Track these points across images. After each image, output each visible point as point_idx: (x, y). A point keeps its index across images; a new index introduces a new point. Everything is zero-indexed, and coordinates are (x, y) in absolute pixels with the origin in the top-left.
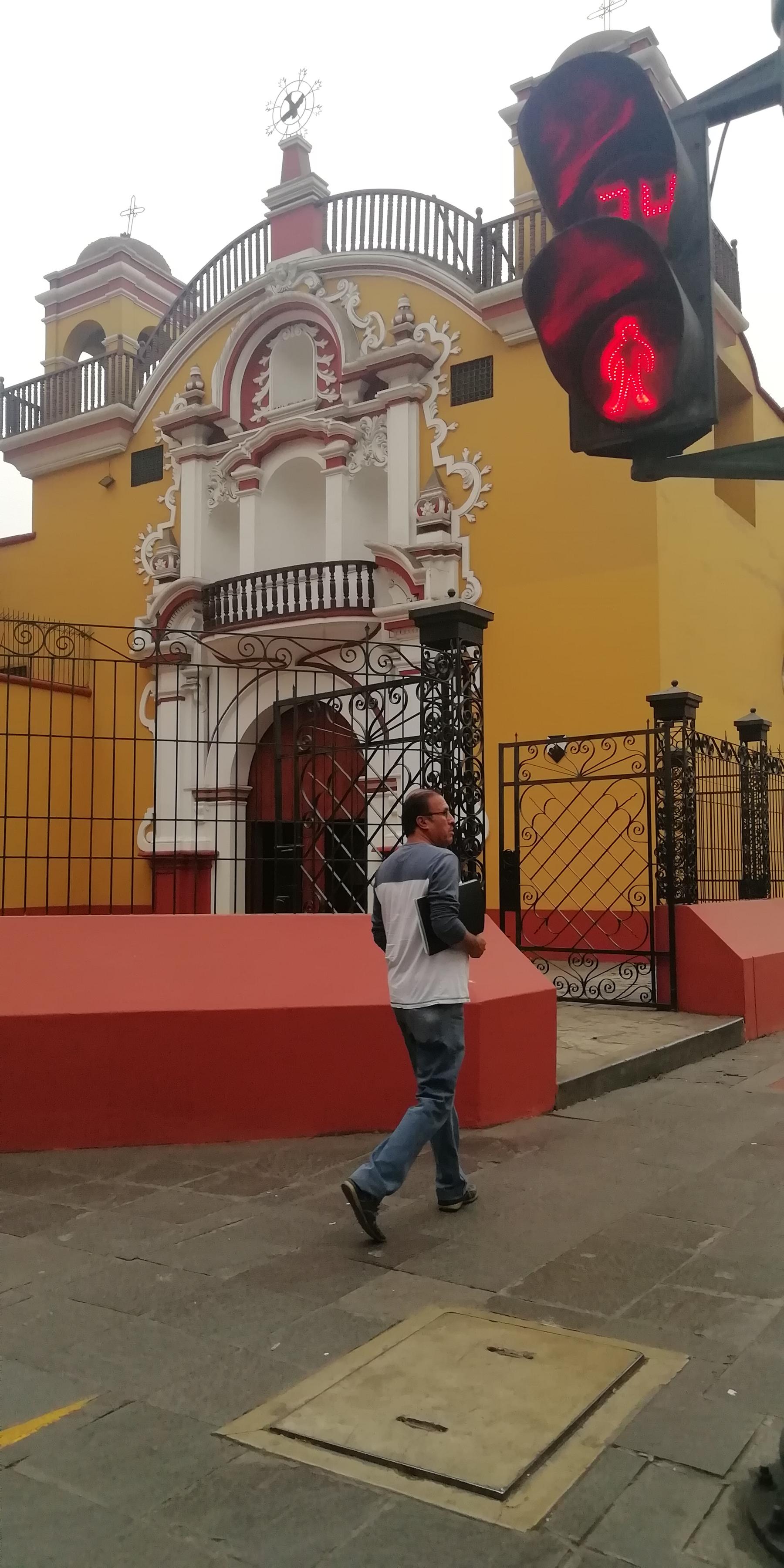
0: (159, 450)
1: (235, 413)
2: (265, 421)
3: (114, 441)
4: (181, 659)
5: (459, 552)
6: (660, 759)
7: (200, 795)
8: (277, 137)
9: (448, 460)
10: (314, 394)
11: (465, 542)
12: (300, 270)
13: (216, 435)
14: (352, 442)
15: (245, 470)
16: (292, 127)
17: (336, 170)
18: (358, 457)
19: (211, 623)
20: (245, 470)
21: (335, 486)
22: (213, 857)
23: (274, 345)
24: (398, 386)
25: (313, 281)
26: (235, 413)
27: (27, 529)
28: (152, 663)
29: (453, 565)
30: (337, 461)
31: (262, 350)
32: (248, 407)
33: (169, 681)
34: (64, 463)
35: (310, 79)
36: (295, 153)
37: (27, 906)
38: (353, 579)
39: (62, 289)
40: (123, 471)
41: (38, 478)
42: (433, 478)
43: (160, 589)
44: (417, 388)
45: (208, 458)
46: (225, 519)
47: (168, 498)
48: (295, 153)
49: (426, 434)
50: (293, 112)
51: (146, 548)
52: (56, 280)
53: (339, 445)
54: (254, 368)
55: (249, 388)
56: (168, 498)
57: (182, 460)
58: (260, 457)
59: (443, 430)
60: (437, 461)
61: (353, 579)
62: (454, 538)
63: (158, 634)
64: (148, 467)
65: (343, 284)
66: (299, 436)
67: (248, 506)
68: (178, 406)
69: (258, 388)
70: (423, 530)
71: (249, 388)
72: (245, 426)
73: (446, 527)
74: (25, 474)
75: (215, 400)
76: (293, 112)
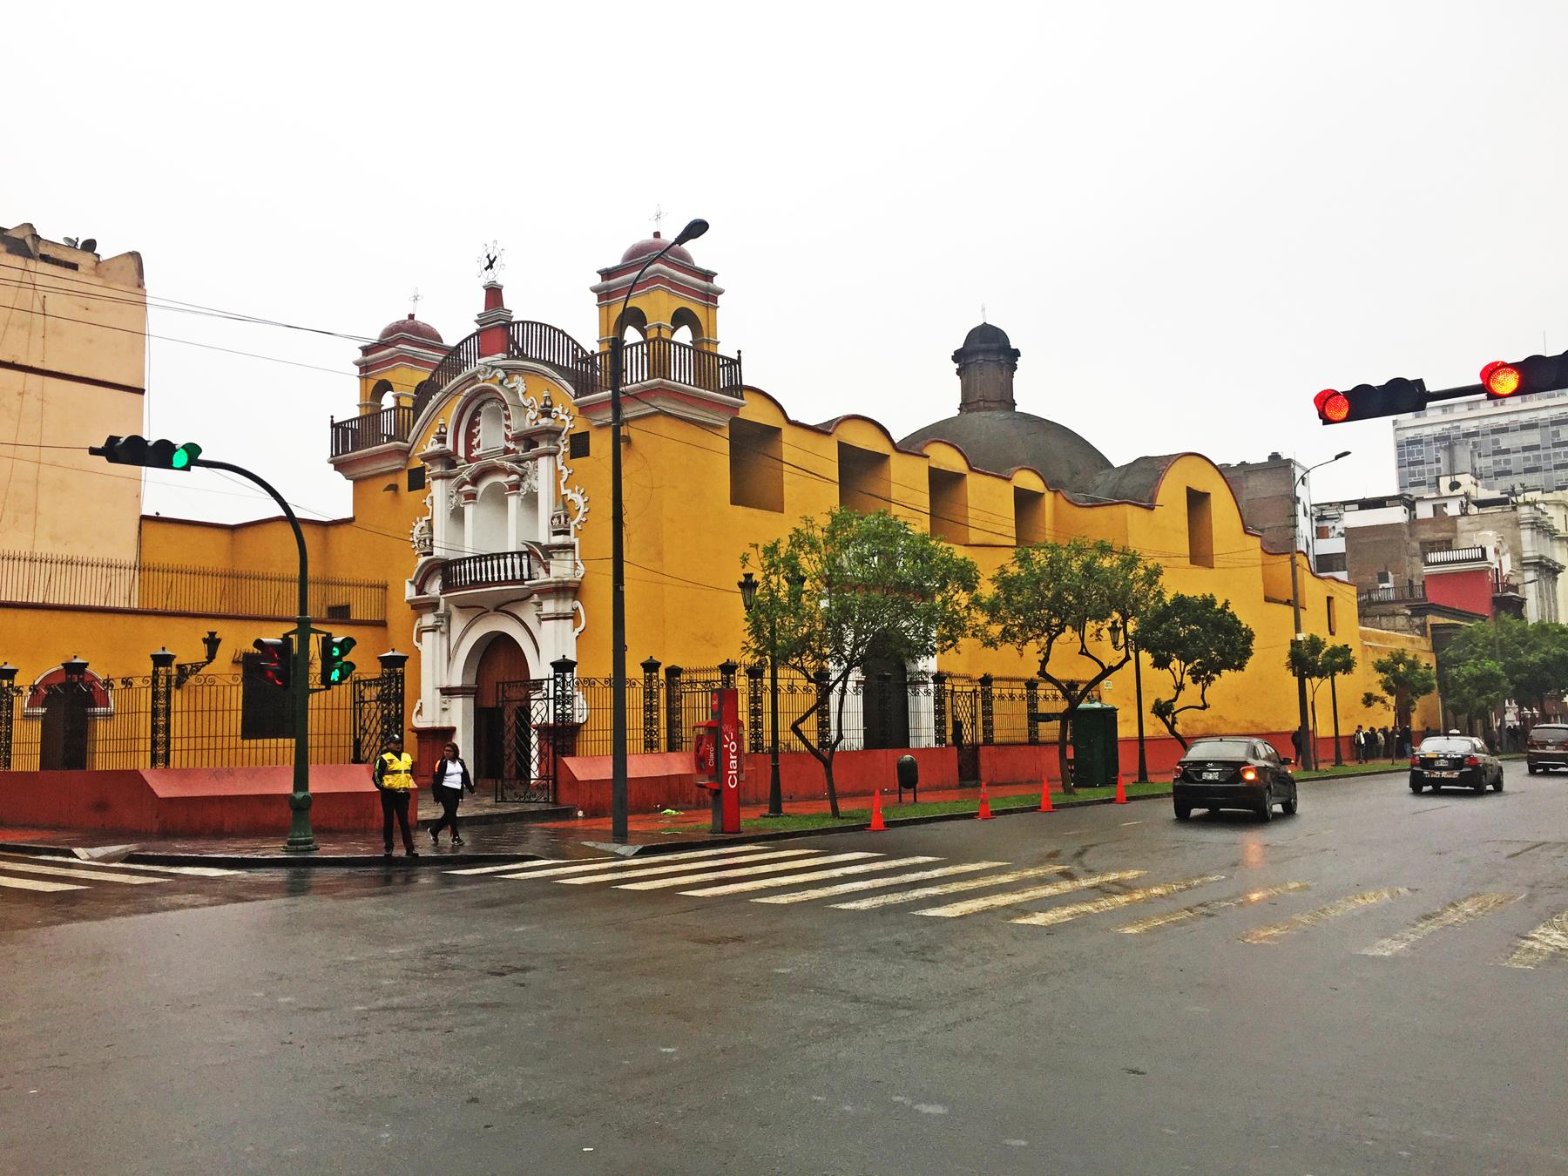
0: (423, 469)
1: (462, 453)
2: (478, 458)
3: (397, 463)
4: (433, 606)
5: (573, 547)
6: (863, 643)
7: (448, 692)
8: (484, 281)
9: (568, 491)
10: (503, 444)
11: (576, 541)
12: (494, 368)
13: (453, 465)
14: (522, 476)
15: (467, 488)
16: (490, 276)
17: (519, 306)
18: (525, 485)
19: (447, 587)
20: (467, 488)
21: (513, 501)
22: (453, 730)
23: (483, 409)
24: (543, 446)
25: (501, 374)
26: (462, 453)
27: (350, 515)
28: (420, 607)
29: (570, 556)
30: (516, 486)
31: (476, 413)
32: (469, 448)
33: (428, 620)
34: (690, 405)
35: (499, 247)
36: (494, 294)
37: (1146, 734)
38: (517, 561)
39: (612, 282)
40: (403, 481)
41: (356, 481)
42: (564, 503)
43: (422, 560)
44: (552, 448)
45: (449, 477)
46: (457, 515)
47: (428, 501)
48: (494, 294)
49: (558, 473)
50: (490, 266)
51: (416, 532)
52: (607, 274)
53: (514, 477)
54: (473, 424)
55: (470, 436)
56: (428, 501)
57: (434, 479)
58: (475, 481)
59: (566, 473)
60: (563, 492)
61: (517, 561)
62: (571, 539)
63: (420, 591)
64: (417, 480)
65: (517, 378)
66: (495, 470)
67: (469, 510)
68: (432, 447)
69: (475, 436)
70: (556, 533)
71: (470, 436)
72: (469, 459)
73: (567, 533)
74: (347, 478)
75: (449, 446)
76: (490, 266)
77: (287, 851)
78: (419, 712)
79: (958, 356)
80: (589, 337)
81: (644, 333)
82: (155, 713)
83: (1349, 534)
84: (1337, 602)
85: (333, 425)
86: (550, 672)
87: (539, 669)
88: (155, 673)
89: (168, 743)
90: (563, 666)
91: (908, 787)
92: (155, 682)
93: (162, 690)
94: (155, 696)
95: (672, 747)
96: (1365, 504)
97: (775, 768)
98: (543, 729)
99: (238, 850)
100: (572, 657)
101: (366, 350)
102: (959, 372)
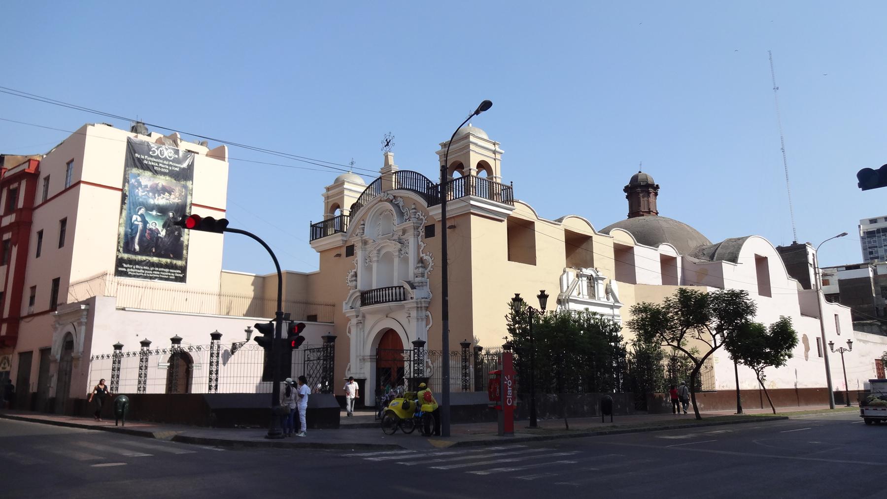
7: (363, 360)
49: (419, 247)
50: (387, 145)
60: (422, 255)
76: (387, 145)
77: (266, 437)
78: (349, 370)
79: (626, 189)
80: (435, 178)
81: (462, 173)
82: (211, 364)
83: (841, 282)
84: (840, 317)
85: (312, 226)
86: (412, 347)
87: (407, 345)
88: (212, 343)
89: (217, 380)
90: (419, 344)
91: (607, 414)
92: (212, 348)
93: (215, 352)
94: (212, 355)
95: (477, 388)
96: (849, 268)
97: (606, 434)
98: (409, 380)
99: (807, 413)
100: (424, 339)
101: (328, 189)
102: (627, 197)
